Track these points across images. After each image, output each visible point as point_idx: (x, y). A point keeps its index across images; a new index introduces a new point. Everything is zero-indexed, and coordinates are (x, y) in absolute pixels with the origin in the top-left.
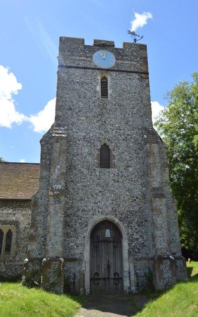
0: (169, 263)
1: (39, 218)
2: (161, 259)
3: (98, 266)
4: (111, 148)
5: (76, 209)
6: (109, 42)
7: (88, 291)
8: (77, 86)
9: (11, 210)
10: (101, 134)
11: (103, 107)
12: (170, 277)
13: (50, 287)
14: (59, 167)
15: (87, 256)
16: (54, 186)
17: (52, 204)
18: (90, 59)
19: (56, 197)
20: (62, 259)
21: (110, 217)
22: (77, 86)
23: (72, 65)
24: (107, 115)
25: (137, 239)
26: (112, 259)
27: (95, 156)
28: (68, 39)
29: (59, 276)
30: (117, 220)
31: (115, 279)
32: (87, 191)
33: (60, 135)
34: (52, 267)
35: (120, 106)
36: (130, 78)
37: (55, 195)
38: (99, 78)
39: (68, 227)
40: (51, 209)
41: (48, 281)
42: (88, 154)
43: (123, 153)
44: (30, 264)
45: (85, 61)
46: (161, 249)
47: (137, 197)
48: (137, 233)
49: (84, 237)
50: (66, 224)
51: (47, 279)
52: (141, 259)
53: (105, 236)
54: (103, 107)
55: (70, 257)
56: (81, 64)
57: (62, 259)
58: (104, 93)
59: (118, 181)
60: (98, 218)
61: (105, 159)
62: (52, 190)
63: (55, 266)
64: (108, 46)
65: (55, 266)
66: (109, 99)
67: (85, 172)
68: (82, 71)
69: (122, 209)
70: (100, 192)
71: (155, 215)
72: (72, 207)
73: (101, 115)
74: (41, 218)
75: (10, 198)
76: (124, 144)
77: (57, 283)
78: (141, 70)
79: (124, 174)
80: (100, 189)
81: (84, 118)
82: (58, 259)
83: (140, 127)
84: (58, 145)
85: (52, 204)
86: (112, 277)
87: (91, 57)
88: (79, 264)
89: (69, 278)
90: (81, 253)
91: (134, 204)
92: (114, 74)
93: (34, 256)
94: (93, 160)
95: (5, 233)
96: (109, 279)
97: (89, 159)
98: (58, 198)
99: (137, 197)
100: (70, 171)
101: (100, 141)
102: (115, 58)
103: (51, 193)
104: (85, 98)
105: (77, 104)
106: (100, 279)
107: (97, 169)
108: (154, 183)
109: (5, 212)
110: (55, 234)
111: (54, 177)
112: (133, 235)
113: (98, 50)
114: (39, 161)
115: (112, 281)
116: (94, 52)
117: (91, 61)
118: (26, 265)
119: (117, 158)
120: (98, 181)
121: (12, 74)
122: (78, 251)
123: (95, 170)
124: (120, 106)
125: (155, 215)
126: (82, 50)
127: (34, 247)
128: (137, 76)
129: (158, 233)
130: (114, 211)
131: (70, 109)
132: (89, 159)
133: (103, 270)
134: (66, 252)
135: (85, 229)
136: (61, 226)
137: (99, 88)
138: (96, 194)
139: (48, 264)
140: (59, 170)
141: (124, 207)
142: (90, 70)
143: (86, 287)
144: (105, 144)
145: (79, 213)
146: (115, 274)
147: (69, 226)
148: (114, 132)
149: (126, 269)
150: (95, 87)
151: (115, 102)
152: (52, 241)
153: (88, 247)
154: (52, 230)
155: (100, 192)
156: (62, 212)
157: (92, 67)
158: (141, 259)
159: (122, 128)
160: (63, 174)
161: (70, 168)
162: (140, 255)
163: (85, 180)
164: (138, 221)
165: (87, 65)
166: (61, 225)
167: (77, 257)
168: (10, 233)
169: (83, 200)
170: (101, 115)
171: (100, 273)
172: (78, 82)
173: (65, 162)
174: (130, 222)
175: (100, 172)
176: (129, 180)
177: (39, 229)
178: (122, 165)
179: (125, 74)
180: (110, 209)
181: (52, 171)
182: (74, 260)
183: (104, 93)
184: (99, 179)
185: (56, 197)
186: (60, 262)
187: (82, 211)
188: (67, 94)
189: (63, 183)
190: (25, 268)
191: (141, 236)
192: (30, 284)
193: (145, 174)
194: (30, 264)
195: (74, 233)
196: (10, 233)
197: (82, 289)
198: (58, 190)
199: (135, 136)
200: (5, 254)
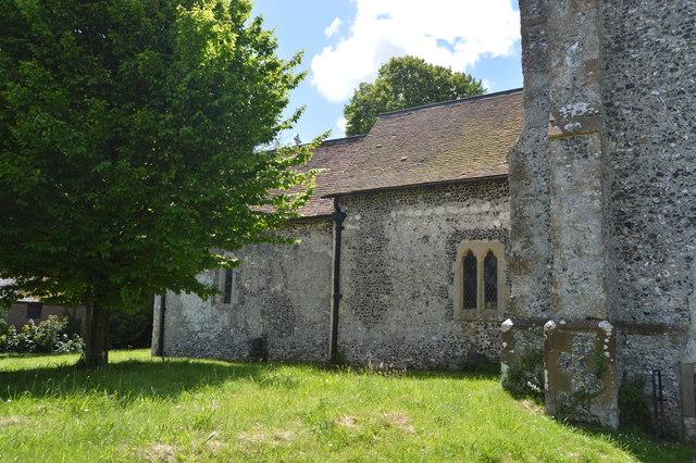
1: (532, 210)
5: (652, 173)
9: (488, 203)
13: (575, 404)
14: (574, 47)
16: (563, 110)
17: (559, 164)
19: (570, 138)
20: (606, 326)
29: (599, 374)
34: (576, 346)
37: (566, 133)
39: (626, 230)
40: (560, 178)
41: (566, 385)
44: (518, 335)
50: (619, 221)
51: (561, 381)
55: (642, 319)
57: (606, 326)
62: (559, 122)
63: (584, 343)
65: (584, 343)
72: (636, 168)
74: (540, 209)
75: (481, 174)
77: (595, 395)
82: (592, 323)
85: (559, 164)
88: (674, 344)
89: (641, 382)
90: (678, 310)
93: (529, 315)
95: (480, 261)
98: (578, 143)
100: (620, 55)
103: (555, 131)
109: (474, 209)
110: (578, 252)
111: (564, 80)
118: (508, 336)
127: (526, 289)
134: (625, 305)
136: (594, 224)
139: (560, 338)
140: (575, 56)
145: (665, 183)
147: (629, 225)
152: (568, 273)
154: (566, 238)
156: (597, 183)
160: (590, 65)
161: (617, 45)
163: (678, 74)
166: (595, 222)
167: (667, 319)
168: (490, 259)
169: (673, 140)
173: (594, 28)
177: (536, 240)
181: (554, 64)
185: (570, 138)
186: (601, 332)
187: (675, 175)
189: (592, 94)
190: (505, 344)
192: (517, 389)
194: (518, 335)
195: (648, 247)
196: (490, 259)
200: (486, 307)
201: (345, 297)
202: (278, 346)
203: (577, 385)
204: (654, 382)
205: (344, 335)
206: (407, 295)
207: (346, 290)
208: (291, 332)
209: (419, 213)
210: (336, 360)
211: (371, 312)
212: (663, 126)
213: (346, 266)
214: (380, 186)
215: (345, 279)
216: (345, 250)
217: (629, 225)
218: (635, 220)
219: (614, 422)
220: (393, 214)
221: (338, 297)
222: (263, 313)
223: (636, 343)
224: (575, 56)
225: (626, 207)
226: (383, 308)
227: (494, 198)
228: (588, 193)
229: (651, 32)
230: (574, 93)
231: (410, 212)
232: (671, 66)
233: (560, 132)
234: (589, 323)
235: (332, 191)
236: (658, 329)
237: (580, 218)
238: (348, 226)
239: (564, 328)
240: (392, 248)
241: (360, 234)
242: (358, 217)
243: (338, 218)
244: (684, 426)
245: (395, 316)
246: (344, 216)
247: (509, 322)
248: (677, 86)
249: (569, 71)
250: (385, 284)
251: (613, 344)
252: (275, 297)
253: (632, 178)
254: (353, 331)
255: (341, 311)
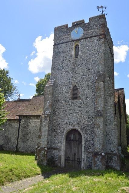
0: (101, 157)
2: (96, 154)
3: (70, 153)
4: (78, 88)
6: (80, 21)
7: (63, 165)
8: (62, 55)
10: (73, 80)
11: (75, 64)
12: (100, 166)
15: (63, 147)
18: (69, 36)
21: (76, 128)
22: (62, 55)
23: (60, 42)
24: (77, 68)
25: (90, 141)
26: (77, 151)
27: (70, 93)
28: (104, 25)
29: (44, 157)
30: (79, 129)
31: (78, 161)
32: (64, 113)
33: (49, 85)
35: (85, 61)
36: (92, 41)
38: (74, 46)
41: (40, 158)
42: (65, 92)
43: (85, 90)
45: (66, 38)
46: (97, 148)
47: (91, 116)
48: (90, 137)
49: (62, 138)
52: (90, 152)
53: (73, 137)
54: (75, 64)
55: (55, 147)
56: (65, 41)
58: (77, 54)
59: (81, 107)
60: (70, 128)
61: (75, 95)
63: (43, 151)
64: (80, 24)
65: (43, 151)
66: (79, 58)
67: (64, 102)
68: (65, 45)
69: (82, 123)
70: (71, 113)
71: (96, 128)
73: (74, 68)
76: (85, 84)
78: (99, 33)
79: (84, 102)
80: (71, 112)
81: (65, 72)
83: (96, 72)
84: (48, 90)
86: (77, 160)
87: (70, 34)
91: (89, 120)
92: (82, 41)
94: (68, 96)
96: (75, 161)
97: (66, 95)
99: (91, 116)
101: (73, 84)
102: (83, 30)
104: (66, 60)
105: (61, 65)
106: (70, 160)
107: (70, 100)
108: (99, 107)
112: (88, 138)
113: (75, 28)
114: (115, 88)
115: (76, 162)
116: (72, 30)
117: (70, 37)
119: (81, 93)
120: (70, 107)
121: (121, 46)
122: (59, 145)
123: (69, 101)
124: (85, 61)
125: (96, 128)
126: (65, 32)
128: (96, 38)
129: (97, 139)
130: (78, 124)
131: (58, 68)
132: (66, 95)
133: (72, 156)
135: (62, 133)
136: (47, 132)
137: (73, 53)
138: (69, 115)
140: (48, 103)
141: (84, 122)
142: (69, 43)
143: (62, 164)
144: (75, 85)
145: (60, 125)
146: (78, 159)
147: (55, 131)
148: (80, 78)
149: (83, 157)
150: (71, 52)
151: (82, 59)
153: (64, 143)
154: (43, 134)
155: (71, 113)
157: (70, 40)
158: (90, 152)
159: (85, 75)
162: (91, 150)
164: (91, 130)
165: (68, 40)
170: (74, 68)
171: (70, 157)
172: (63, 52)
174: (86, 131)
175: (72, 102)
176: (87, 106)
178: (83, 97)
179: (89, 39)
180: (76, 123)
182: (56, 149)
183: (77, 54)
184: (71, 106)
188: (57, 60)
189: (50, 110)
191: (92, 139)
193: (95, 103)
197: (59, 164)
198: (47, 114)
199: (92, 78)
201: (20, 137)
202: (6, 148)
203: (41, 158)
205: (19, 146)
206: (32, 137)
207: (20, 136)
208: (9, 144)
209: (35, 121)
210: (17, 152)
211: (25, 141)
213: (21, 131)
214: (28, 114)
215: (20, 133)
216: (21, 127)
217: (55, 131)
219: (119, 169)
220: (30, 120)
221: (18, 137)
222: (3, 140)
224: (48, 103)
225: (55, 128)
226: (27, 140)
228: (46, 127)
231: (33, 120)
232: (63, 106)
235: (19, 114)
238: (22, 122)
239: (41, 149)
240: (30, 128)
241: (24, 124)
242: (24, 120)
243: (20, 120)
245: (29, 141)
246: (21, 120)
248: (64, 109)
250: (28, 135)
252: (6, 136)
253: (56, 124)
254: (21, 145)
255: (19, 140)
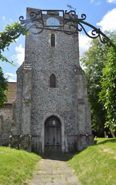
1: (17, 114)
5: (37, 110)
16: (25, 97)
19: (26, 103)
29: (29, 144)
37: (26, 102)
44: (13, 138)
57: (30, 136)
63: (27, 139)
65: (27, 139)
90: (39, 133)
118: (11, 139)
139: (23, 138)
145: (39, 112)
147: (33, 119)
154: (25, 121)
156: (30, 111)
160: (30, 90)
161: (34, 87)
163: (42, 94)
169: (40, 105)
177: (17, 120)
186: (29, 137)
189: (30, 96)
190: (10, 140)
192: (12, 147)
194: (13, 138)
195: (36, 122)
204: (55, 30)
212: (39, 102)
218: (34, 118)
223: (34, 139)
227: (10, 108)
229: (39, 86)
230: (27, 95)
233: (25, 102)
234: (28, 135)
236: (36, 136)
237: (27, 117)
244: (39, 152)
247: (11, 136)
249: (26, 91)
251: (31, 139)
